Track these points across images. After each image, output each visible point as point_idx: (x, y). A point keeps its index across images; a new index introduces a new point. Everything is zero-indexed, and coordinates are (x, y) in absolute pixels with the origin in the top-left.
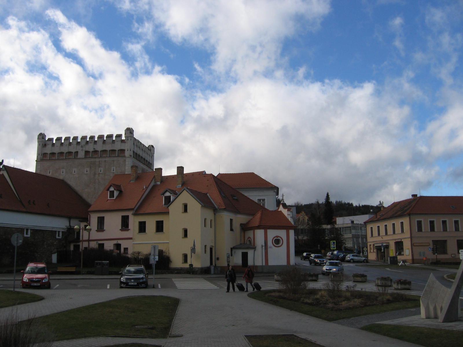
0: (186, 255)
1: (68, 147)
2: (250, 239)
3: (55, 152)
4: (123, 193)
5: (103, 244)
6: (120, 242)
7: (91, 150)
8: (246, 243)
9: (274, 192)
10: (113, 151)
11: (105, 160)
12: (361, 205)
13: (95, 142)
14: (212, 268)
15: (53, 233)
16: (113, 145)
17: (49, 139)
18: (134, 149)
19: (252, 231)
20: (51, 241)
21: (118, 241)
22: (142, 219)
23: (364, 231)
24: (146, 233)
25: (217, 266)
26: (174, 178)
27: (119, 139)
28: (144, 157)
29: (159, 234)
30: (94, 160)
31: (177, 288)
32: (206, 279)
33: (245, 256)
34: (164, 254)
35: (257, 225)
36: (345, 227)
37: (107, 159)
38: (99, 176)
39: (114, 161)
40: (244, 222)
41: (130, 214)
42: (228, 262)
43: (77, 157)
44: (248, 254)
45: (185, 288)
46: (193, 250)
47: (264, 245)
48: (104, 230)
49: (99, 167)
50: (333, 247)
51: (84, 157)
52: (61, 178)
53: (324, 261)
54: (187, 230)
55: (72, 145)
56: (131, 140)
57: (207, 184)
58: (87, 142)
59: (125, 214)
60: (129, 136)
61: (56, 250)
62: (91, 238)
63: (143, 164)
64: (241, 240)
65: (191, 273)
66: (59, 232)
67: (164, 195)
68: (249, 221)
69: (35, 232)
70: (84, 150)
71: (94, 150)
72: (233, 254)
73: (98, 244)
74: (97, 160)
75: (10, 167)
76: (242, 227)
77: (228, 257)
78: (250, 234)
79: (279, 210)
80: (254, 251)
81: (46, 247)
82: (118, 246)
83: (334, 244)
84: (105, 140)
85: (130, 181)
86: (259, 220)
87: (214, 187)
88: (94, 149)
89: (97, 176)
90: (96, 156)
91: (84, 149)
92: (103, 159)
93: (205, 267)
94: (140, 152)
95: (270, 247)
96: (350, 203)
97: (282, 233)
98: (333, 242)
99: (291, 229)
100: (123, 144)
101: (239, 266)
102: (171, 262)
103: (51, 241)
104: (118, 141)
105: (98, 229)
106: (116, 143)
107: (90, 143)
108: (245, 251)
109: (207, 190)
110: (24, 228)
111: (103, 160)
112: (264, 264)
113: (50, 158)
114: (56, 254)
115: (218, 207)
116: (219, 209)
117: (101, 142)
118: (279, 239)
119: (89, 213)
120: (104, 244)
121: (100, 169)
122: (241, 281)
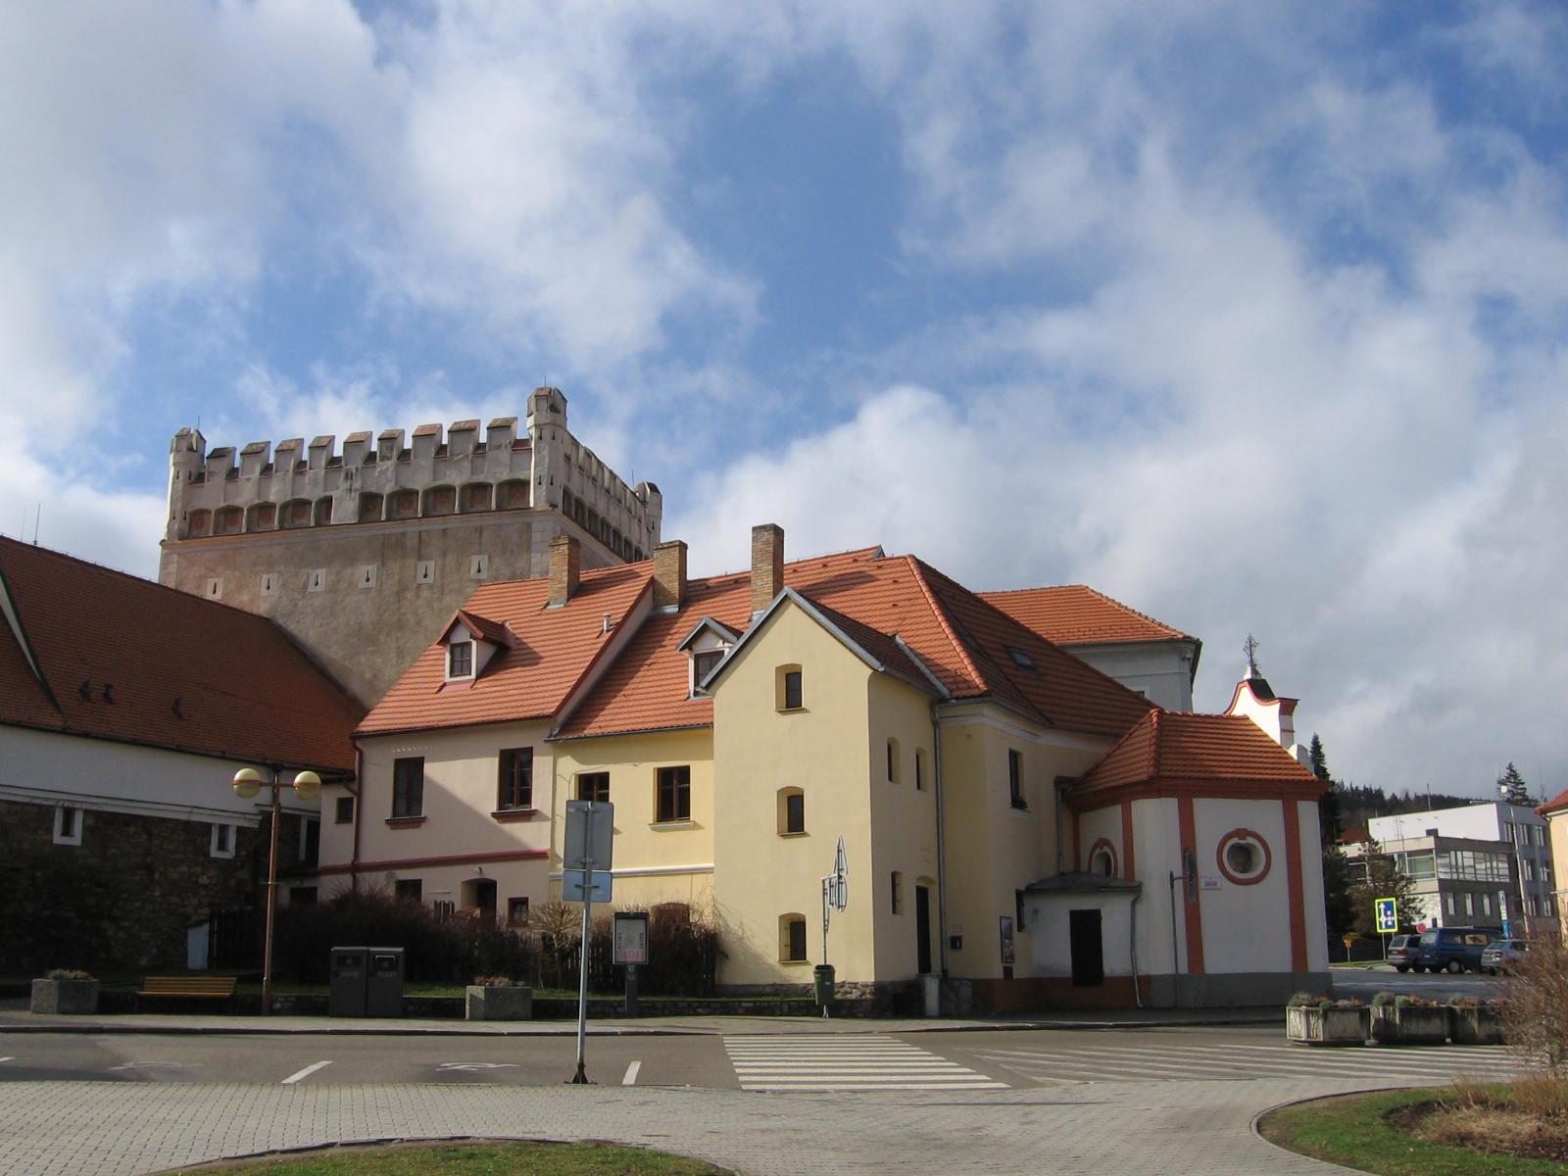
0: (796, 923)
1: (294, 481)
2: (1106, 849)
3: (238, 502)
5: (416, 885)
6: (491, 871)
7: (388, 489)
8: (1084, 868)
9: (1183, 659)
11: (443, 527)
12: (1412, 796)
13: (405, 454)
14: (932, 987)
15: (194, 833)
17: (215, 450)
18: (569, 480)
19: (1116, 812)
20: (183, 868)
21: (484, 866)
23: (1484, 867)
25: (950, 976)
28: (614, 524)
31: (734, 1086)
32: (907, 1037)
33: (1086, 931)
34: (694, 918)
35: (1144, 777)
36: (1411, 854)
38: (418, 597)
39: (480, 530)
40: (1075, 770)
42: (1008, 958)
43: (327, 523)
44: (1101, 918)
45: (909, 1086)
46: (834, 890)
47: (1178, 872)
49: (420, 558)
50: (1386, 923)
52: (262, 608)
54: (804, 924)
56: (553, 438)
57: (892, 599)
58: (371, 457)
59: (515, 741)
61: (206, 911)
62: (368, 857)
63: (613, 550)
64: (1060, 854)
66: (223, 829)
68: (1098, 766)
69: (107, 824)
70: (356, 490)
72: (1027, 921)
73: (394, 880)
75: (20, 544)
76: (1063, 791)
77: (1006, 935)
78: (1106, 823)
79: (1237, 712)
80: (1134, 903)
81: (157, 894)
82: (484, 891)
83: (1389, 913)
84: (446, 446)
85: (548, 604)
86: (1152, 755)
87: (922, 601)
93: (893, 983)
94: (591, 497)
95: (1207, 884)
96: (1371, 790)
97: (1264, 818)
98: (1385, 903)
99: (1306, 796)
101: (1057, 981)
102: (726, 956)
103: (183, 868)
104: (499, 447)
105: (395, 813)
106: (490, 454)
107: (384, 458)
108: (1086, 904)
109: (895, 623)
110: (51, 803)
111: (435, 525)
112: (1184, 969)
114: (206, 928)
115: (951, 691)
116: (957, 698)
117: (426, 461)
118: (1253, 846)
119: (358, 744)
120: (420, 881)
121: (421, 566)
122: (1148, 1046)
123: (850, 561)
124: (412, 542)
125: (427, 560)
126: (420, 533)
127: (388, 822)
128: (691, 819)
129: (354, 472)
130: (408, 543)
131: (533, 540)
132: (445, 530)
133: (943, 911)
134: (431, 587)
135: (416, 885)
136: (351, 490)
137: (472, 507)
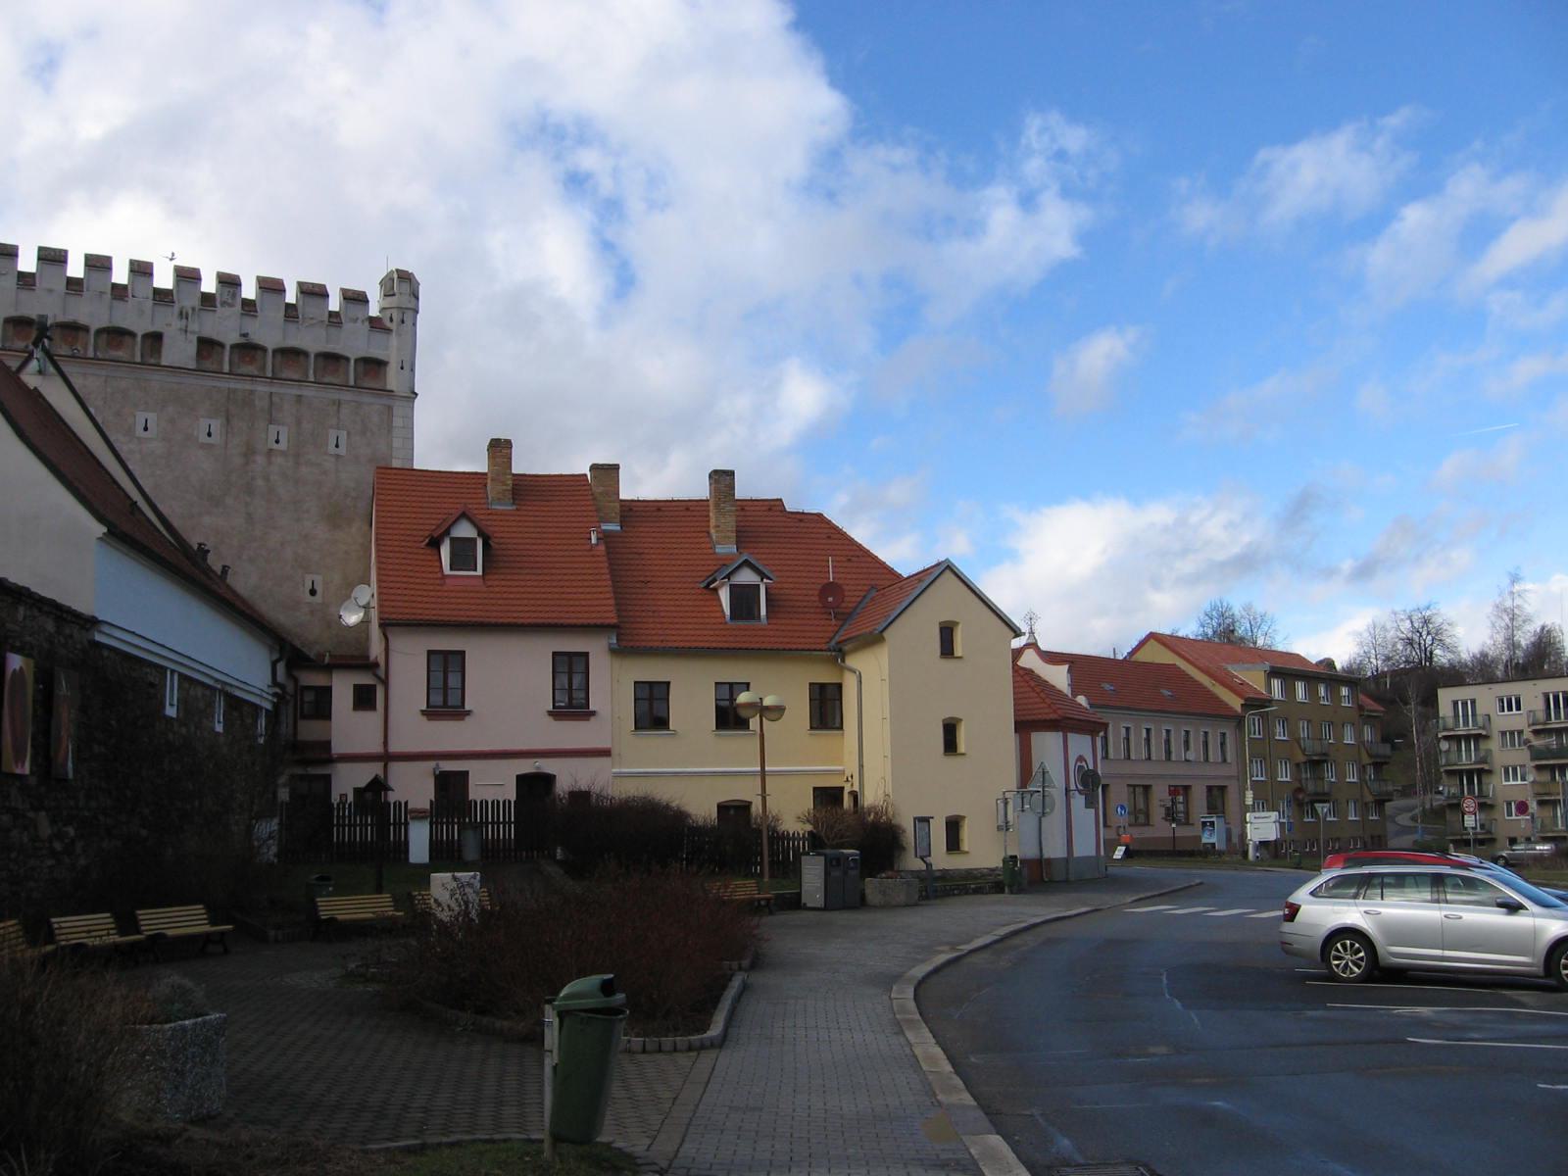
2: (1084, 764)
6: (548, 766)
7: (231, 338)
10: (332, 359)
11: (299, 393)
16: (333, 330)
22: (652, 671)
24: (675, 733)
26: (660, 514)
27: (355, 310)
29: (730, 735)
30: (248, 386)
37: (309, 392)
38: (270, 463)
39: (339, 403)
41: (597, 649)
51: (192, 365)
53: (1128, 854)
60: (410, 306)
62: (395, 747)
65: (1006, 890)
67: (732, 579)
71: (243, 340)
74: (262, 389)
88: (245, 335)
89: (260, 460)
90: (251, 369)
91: (194, 326)
100: (379, 336)
106: (347, 326)
107: (224, 304)
113: (7, 345)
117: (273, 315)
120: (467, 772)
121: (273, 429)
123: (764, 508)
125: (279, 424)
128: (671, 728)
129: (190, 312)
130: (257, 402)
132: (300, 396)
133: (1132, 796)
134: (283, 453)
136: (186, 331)
137: (323, 376)
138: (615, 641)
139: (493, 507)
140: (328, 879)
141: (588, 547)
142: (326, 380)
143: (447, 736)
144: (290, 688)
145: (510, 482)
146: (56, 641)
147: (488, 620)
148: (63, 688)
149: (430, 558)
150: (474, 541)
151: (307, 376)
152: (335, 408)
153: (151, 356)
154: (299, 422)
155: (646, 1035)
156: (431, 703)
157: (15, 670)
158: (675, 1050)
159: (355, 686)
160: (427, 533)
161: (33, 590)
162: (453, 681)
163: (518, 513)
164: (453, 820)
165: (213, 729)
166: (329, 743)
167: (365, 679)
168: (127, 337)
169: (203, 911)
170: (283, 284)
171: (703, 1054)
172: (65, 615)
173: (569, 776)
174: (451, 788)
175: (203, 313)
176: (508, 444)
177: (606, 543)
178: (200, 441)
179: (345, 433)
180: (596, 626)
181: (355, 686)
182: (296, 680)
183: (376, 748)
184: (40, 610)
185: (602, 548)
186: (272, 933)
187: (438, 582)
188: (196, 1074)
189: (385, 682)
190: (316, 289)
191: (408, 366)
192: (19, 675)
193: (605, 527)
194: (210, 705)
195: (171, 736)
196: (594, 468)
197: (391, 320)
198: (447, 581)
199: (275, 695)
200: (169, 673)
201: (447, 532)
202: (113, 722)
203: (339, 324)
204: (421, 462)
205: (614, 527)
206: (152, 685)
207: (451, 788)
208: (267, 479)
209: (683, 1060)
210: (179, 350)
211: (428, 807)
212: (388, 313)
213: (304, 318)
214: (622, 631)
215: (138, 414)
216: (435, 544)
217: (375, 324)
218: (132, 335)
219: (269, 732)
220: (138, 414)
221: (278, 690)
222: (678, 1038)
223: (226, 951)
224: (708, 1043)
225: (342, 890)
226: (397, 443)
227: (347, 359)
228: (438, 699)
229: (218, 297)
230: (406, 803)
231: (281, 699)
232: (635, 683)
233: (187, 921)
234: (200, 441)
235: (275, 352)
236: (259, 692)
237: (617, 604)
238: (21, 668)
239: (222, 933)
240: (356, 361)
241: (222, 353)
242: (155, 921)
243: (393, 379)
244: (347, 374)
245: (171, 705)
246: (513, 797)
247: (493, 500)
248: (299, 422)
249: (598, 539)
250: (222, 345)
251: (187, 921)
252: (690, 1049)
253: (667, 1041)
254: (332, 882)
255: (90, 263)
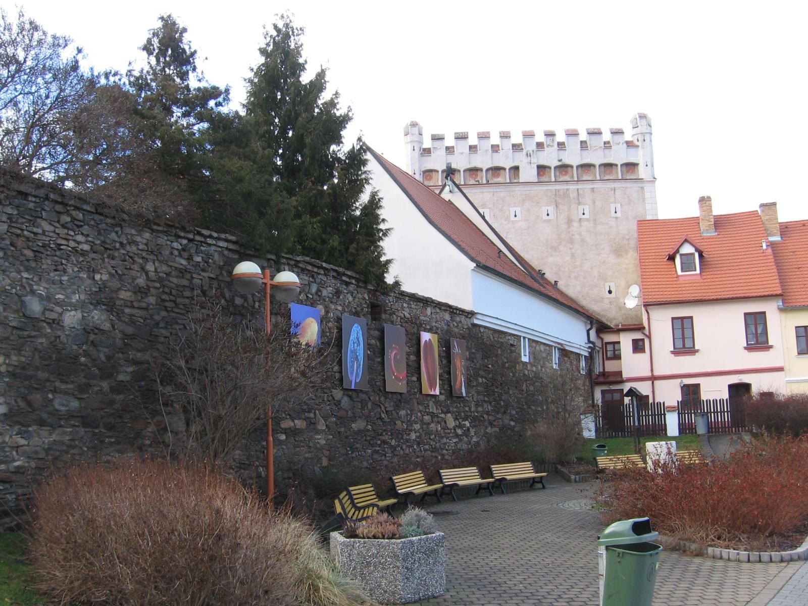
4: (705, 260)
5: (697, 386)
7: (553, 163)
10: (608, 166)
16: (607, 151)
26: (805, 228)
27: (618, 138)
37: (598, 186)
41: (771, 309)
48: (697, 351)
49: (579, 204)
51: (536, 181)
54: (621, 372)
55: (501, 151)
62: (657, 373)
71: (560, 163)
74: (572, 187)
88: (560, 161)
89: (575, 224)
90: (567, 178)
92: (589, 186)
100: (632, 151)
107: (548, 146)
113: (625, 177)
117: (573, 146)
120: (699, 384)
121: (581, 208)
124: (573, 195)
125: (584, 205)
126: (578, 189)
127: (672, 352)
130: (571, 195)
131: (646, 197)
134: (588, 220)
135: (697, 386)
138: (781, 304)
139: (704, 235)
140: (604, 446)
141: (762, 251)
142: (606, 178)
143: (686, 364)
144: (599, 344)
145: (713, 220)
146: (452, 325)
147: (705, 298)
148: (456, 350)
149: (669, 266)
150: (693, 254)
151: (596, 178)
152: (613, 192)
153: (515, 179)
154: (594, 202)
155: (760, 550)
156: (676, 347)
157: (426, 341)
158: (771, 561)
159: (633, 340)
160: (667, 253)
161: (434, 299)
162: (687, 333)
163: (719, 236)
164: (691, 411)
165: (552, 367)
166: (621, 372)
167: (638, 336)
168: (501, 171)
169: (531, 465)
170: (577, 131)
171: (792, 564)
172: (455, 311)
173: (759, 384)
174: (691, 393)
175: (539, 152)
176: (709, 199)
177: (772, 248)
178: (544, 218)
179: (619, 205)
180: (768, 296)
181: (633, 340)
182: (602, 339)
183: (649, 374)
184: (440, 309)
185: (770, 251)
186: (573, 477)
187: (675, 279)
188: (422, 570)
189: (649, 337)
190: (596, 131)
191: (650, 165)
192: (429, 344)
193: (771, 239)
194: (550, 354)
195: (526, 372)
196: (762, 206)
197: (638, 140)
198: (680, 278)
199: (590, 347)
200: (522, 338)
201: (677, 251)
202: (490, 366)
203: (610, 147)
204: (662, 216)
205: (777, 238)
206: (512, 345)
207: (691, 393)
208: (580, 234)
209: (773, 568)
210: (528, 173)
211: (676, 405)
212: (636, 137)
213: (591, 147)
214: (785, 298)
215: (511, 209)
216: (672, 258)
217: (629, 144)
218: (504, 169)
219: (588, 368)
220: (511, 209)
221: (591, 345)
222: (772, 553)
223: (544, 487)
224: (796, 557)
225: (612, 452)
226: (648, 206)
227: (616, 165)
228: (679, 344)
229: (545, 143)
230: (664, 403)
231: (592, 350)
232: (796, 327)
233: (522, 470)
234: (544, 218)
235: (577, 167)
236: (579, 347)
237: (781, 283)
238: (430, 339)
239: (541, 477)
240: (622, 165)
241: (550, 171)
242: (502, 471)
243: (642, 172)
244: (617, 173)
245: (525, 355)
246: (727, 396)
247: (703, 230)
248: (594, 202)
249: (767, 246)
250: (549, 168)
251: (522, 470)
252: (782, 561)
253: (765, 555)
254: (607, 448)
255: (480, 136)
